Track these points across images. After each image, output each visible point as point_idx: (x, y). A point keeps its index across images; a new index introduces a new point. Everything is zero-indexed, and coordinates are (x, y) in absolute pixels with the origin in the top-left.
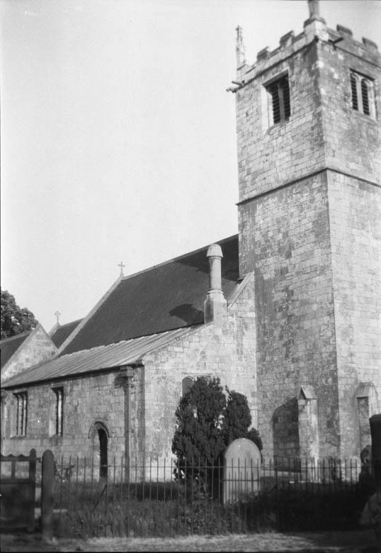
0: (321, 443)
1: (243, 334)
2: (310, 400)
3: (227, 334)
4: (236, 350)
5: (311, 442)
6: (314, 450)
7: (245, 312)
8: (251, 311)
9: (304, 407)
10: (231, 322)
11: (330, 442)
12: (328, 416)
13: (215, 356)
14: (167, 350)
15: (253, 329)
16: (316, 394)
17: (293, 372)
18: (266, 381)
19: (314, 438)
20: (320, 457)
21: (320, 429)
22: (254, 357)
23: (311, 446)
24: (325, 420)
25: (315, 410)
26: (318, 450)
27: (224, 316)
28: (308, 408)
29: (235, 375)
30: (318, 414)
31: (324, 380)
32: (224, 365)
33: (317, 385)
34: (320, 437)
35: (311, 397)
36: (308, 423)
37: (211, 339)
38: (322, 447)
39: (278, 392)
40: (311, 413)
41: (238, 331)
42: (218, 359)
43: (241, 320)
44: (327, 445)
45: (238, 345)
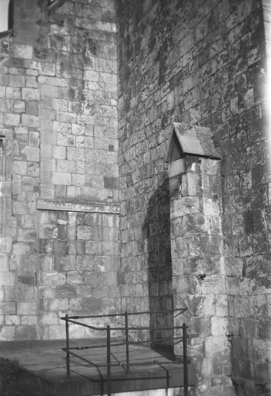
0: (233, 279)
1: (87, 61)
2: (196, 157)
3: (45, 57)
4: (66, 91)
5: (202, 277)
6: (210, 299)
7: (93, 22)
8: (106, 19)
9: (179, 177)
10: (55, 36)
11: (253, 275)
12: (247, 200)
13: (16, 101)
14: (46, 181)
15: (110, 51)
16: (216, 144)
17: (172, 111)
18: (132, 150)
19: (212, 266)
20: (229, 317)
21: (229, 241)
22: (114, 105)
23: (202, 289)
24: (238, 208)
25: (214, 189)
26: (223, 300)
27: (39, 22)
28: (190, 181)
29: (63, 141)
30: (221, 195)
31: (234, 102)
32: (35, 118)
33: (219, 122)
34: (230, 262)
35: (200, 151)
36: (193, 223)
37: (5, 65)
38: (234, 291)
39: (149, 167)
40: (200, 195)
41: (72, 53)
42: (21, 106)
43: (82, 33)
44: (246, 285)
45: (73, 81)
